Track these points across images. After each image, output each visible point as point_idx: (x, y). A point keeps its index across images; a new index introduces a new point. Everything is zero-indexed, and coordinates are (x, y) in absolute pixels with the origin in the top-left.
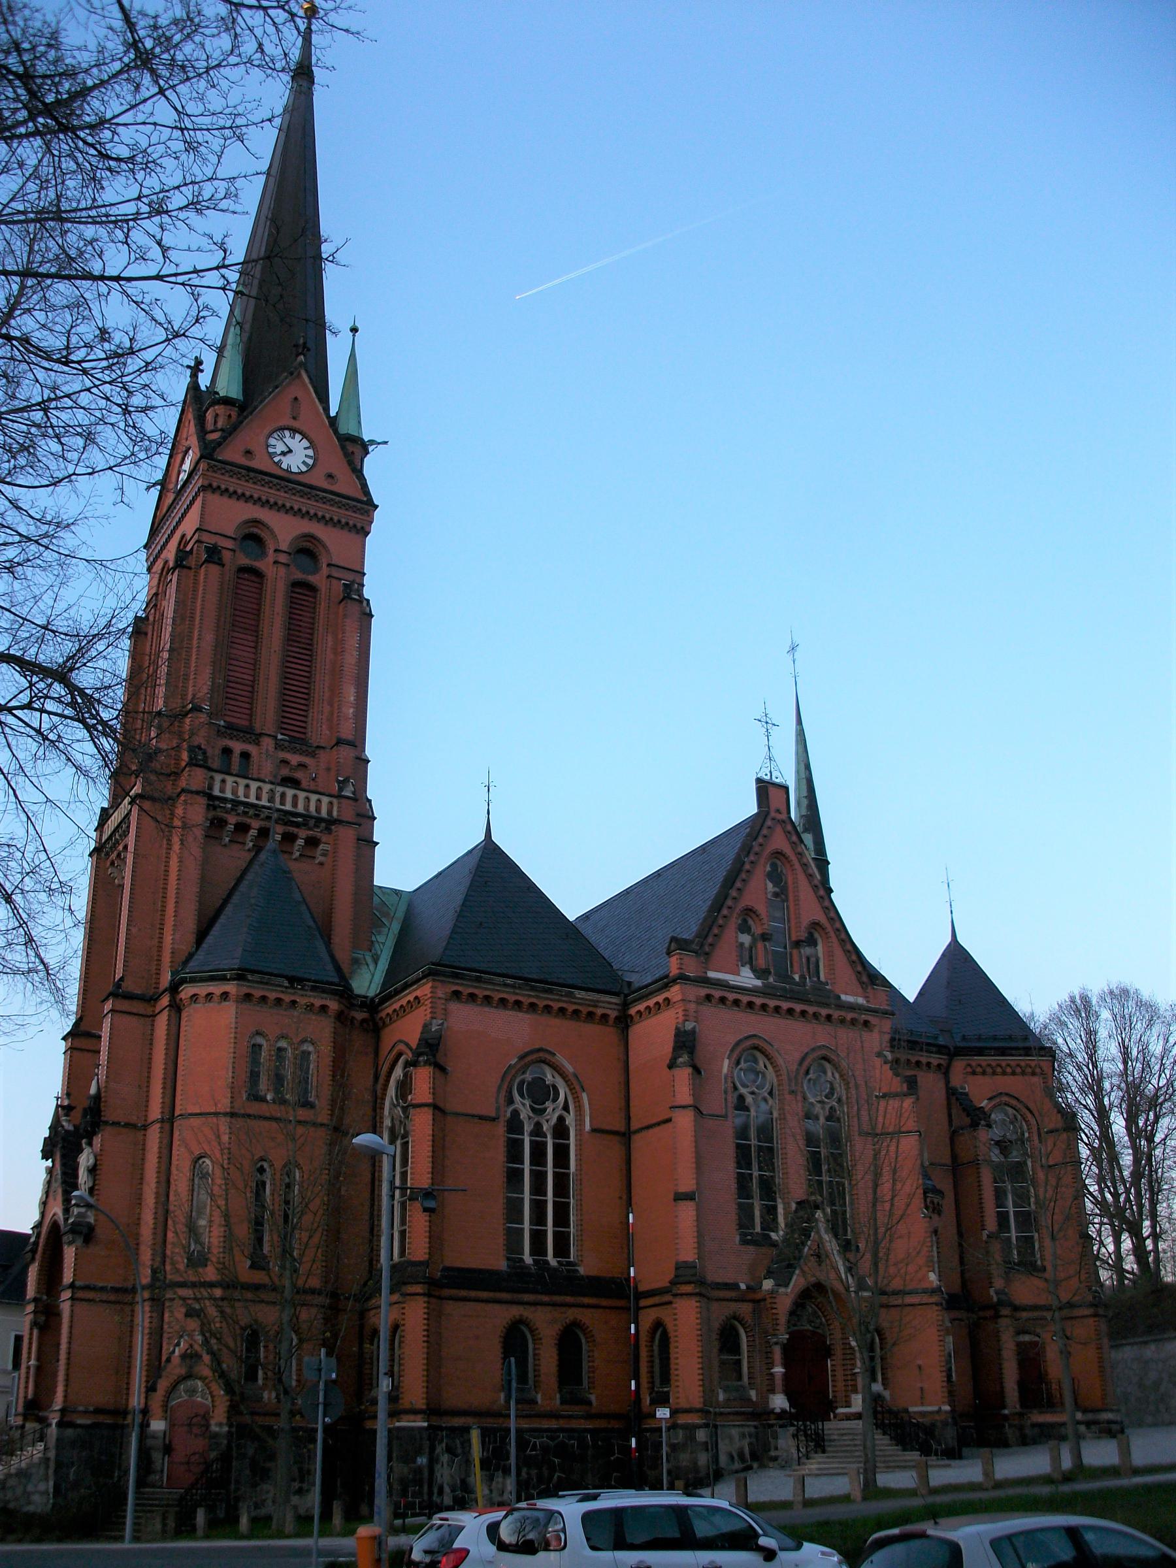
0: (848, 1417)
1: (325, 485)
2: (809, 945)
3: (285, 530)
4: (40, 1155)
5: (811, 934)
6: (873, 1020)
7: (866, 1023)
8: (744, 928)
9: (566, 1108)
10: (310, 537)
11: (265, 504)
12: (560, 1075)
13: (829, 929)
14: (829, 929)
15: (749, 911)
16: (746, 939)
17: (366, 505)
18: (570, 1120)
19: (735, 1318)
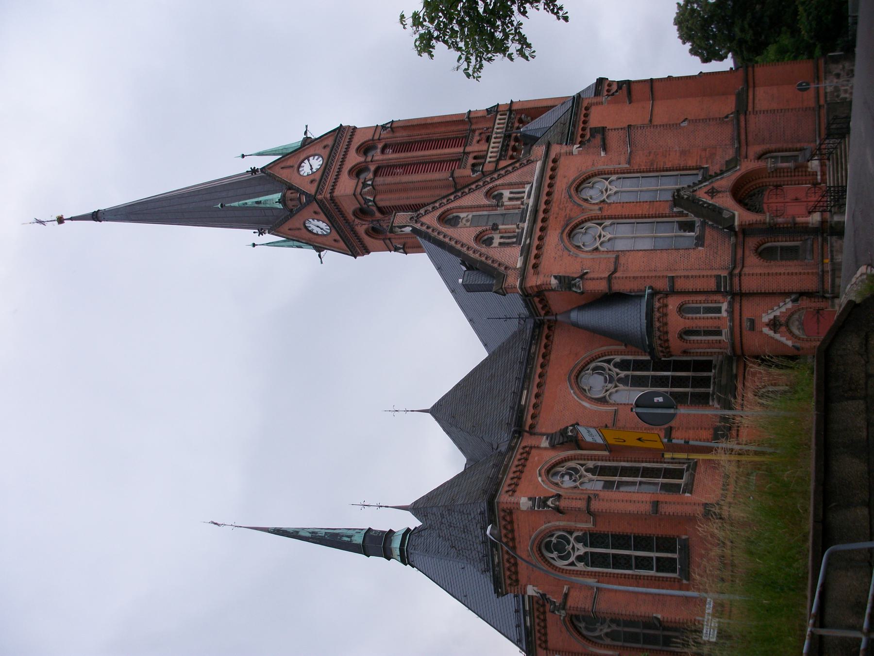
0: (823, 174)
1: (316, 184)
2: (502, 198)
3: (354, 159)
4: (680, 41)
5: (494, 197)
6: (552, 155)
7: (555, 161)
8: (489, 242)
9: (608, 362)
10: (350, 172)
11: (340, 169)
12: (586, 365)
13: (491, 185)
14: (491, 185)
15: (478, 238)
16: (497, 241)
17: (340, 130)
18: (618, 359)
19: (756, 250)
